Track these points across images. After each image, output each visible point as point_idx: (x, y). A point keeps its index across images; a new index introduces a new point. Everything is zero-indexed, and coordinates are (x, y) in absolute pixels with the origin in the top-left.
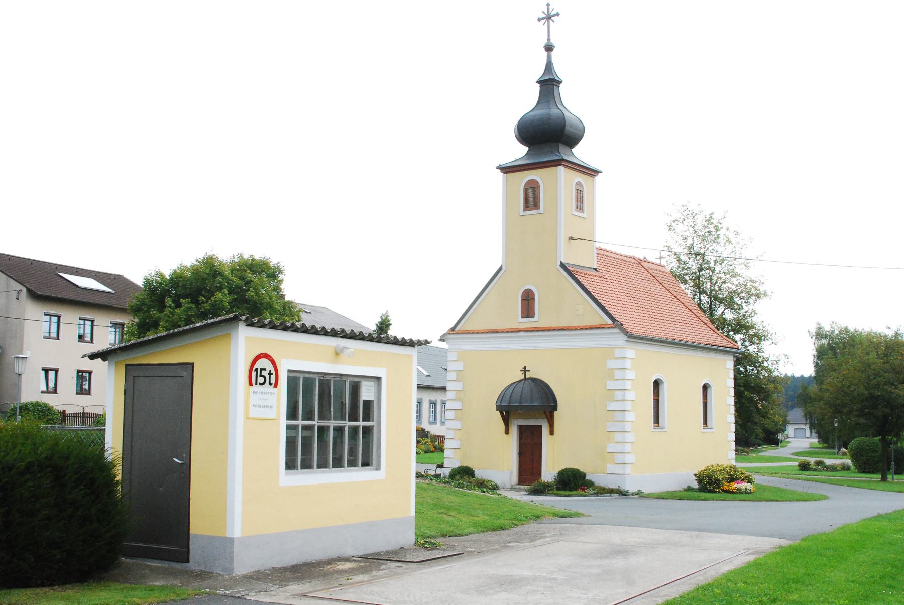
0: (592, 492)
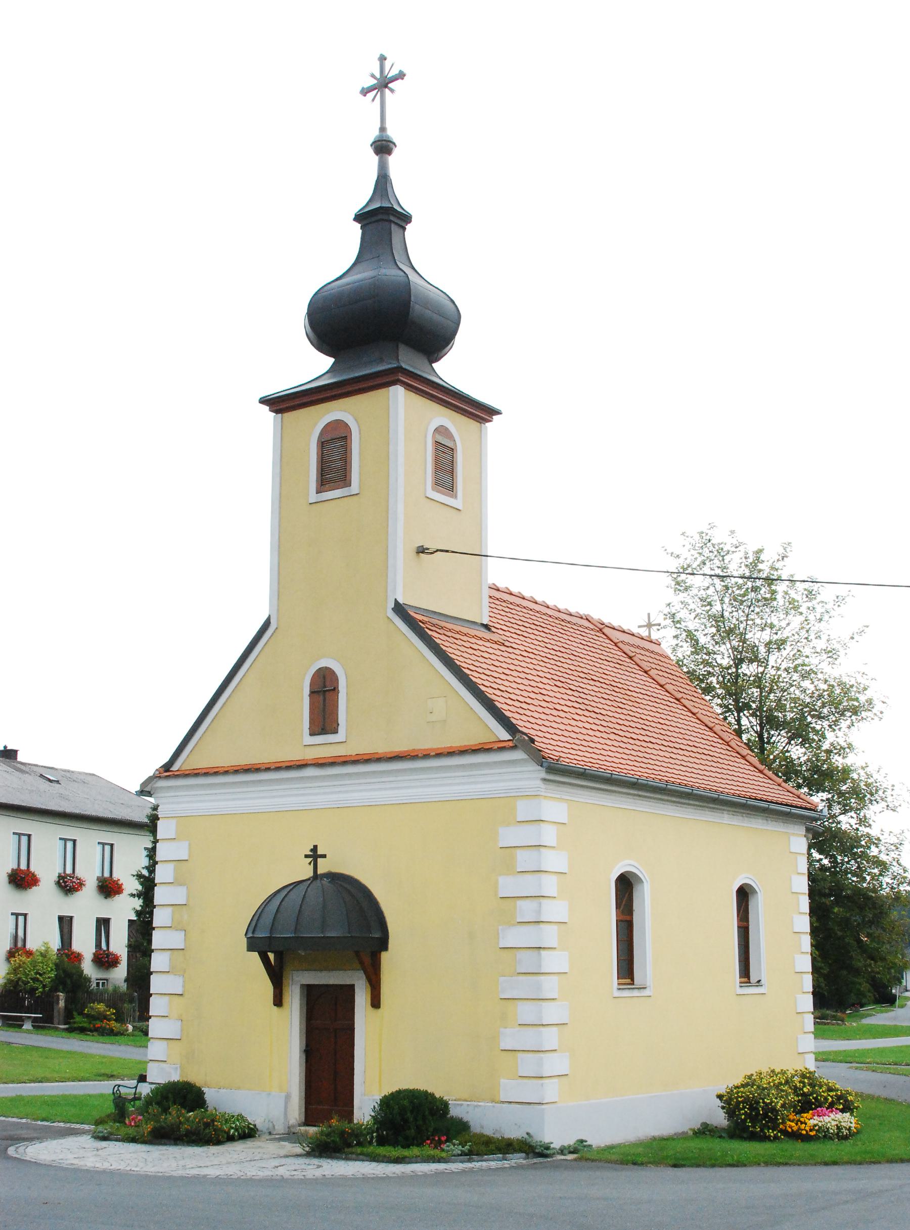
0: (458, 1149)
